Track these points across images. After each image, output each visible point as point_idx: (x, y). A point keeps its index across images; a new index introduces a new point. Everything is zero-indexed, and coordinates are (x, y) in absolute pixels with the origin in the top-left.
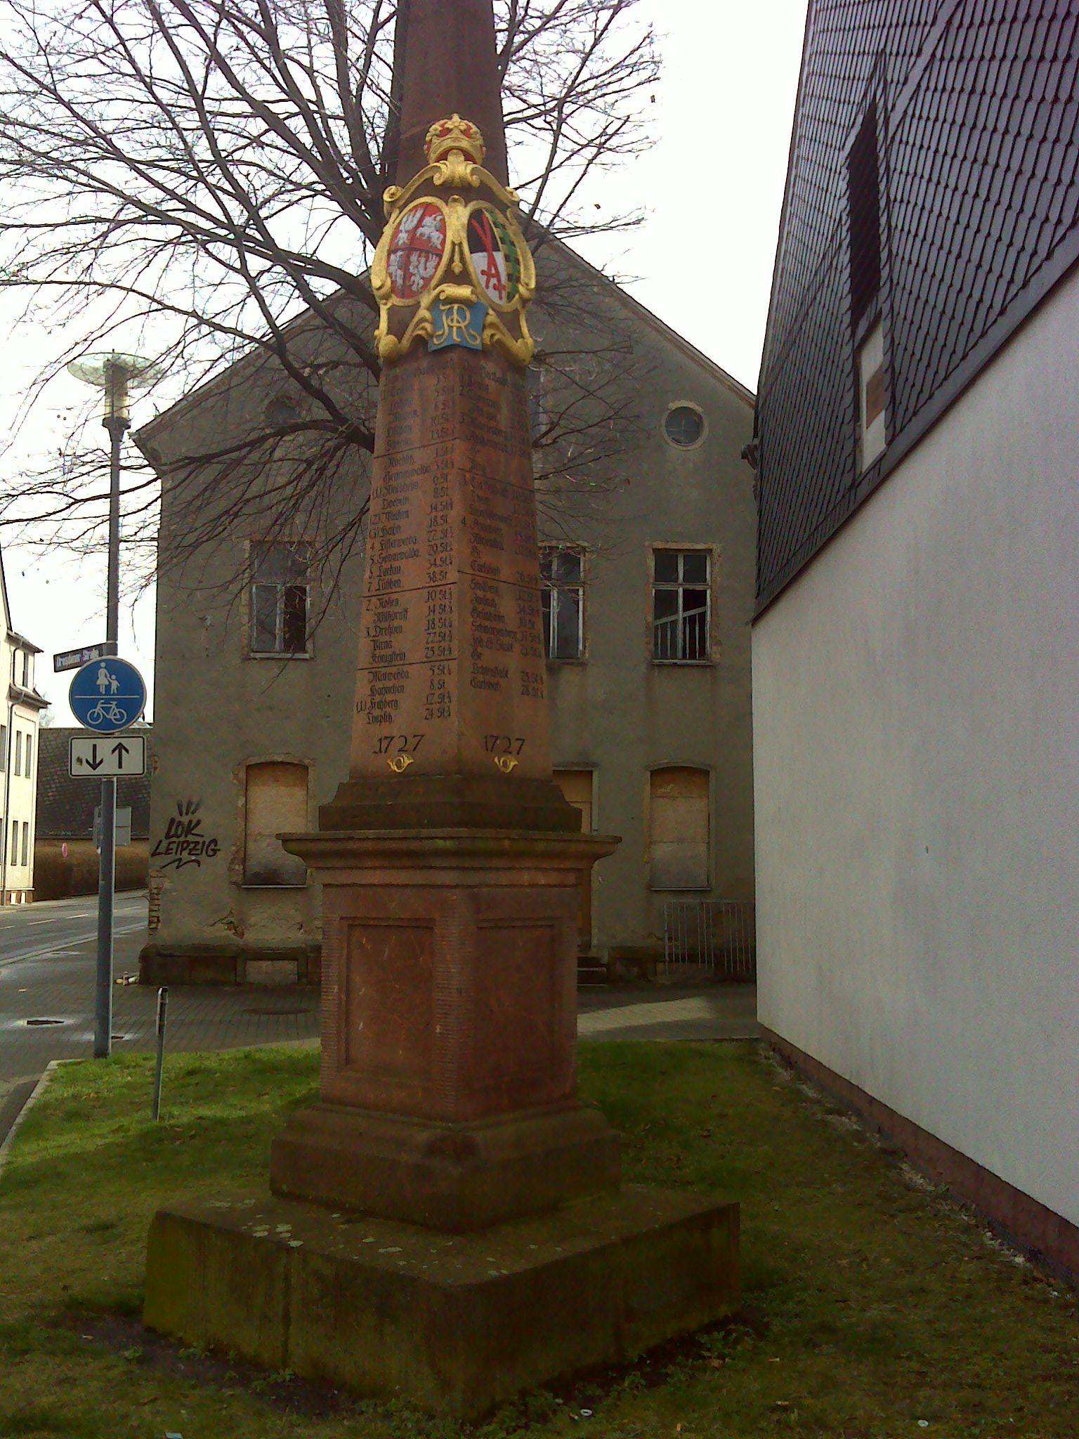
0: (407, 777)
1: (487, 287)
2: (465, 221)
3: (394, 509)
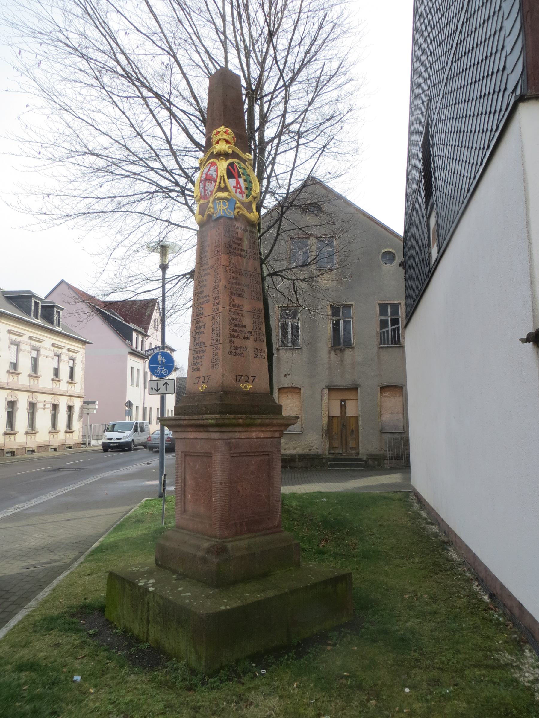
0: (205, 393)
1: (236, 192)
2: (226, 167)
3: (202, 284)
